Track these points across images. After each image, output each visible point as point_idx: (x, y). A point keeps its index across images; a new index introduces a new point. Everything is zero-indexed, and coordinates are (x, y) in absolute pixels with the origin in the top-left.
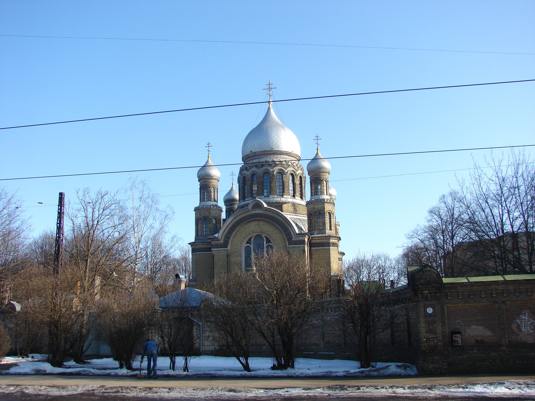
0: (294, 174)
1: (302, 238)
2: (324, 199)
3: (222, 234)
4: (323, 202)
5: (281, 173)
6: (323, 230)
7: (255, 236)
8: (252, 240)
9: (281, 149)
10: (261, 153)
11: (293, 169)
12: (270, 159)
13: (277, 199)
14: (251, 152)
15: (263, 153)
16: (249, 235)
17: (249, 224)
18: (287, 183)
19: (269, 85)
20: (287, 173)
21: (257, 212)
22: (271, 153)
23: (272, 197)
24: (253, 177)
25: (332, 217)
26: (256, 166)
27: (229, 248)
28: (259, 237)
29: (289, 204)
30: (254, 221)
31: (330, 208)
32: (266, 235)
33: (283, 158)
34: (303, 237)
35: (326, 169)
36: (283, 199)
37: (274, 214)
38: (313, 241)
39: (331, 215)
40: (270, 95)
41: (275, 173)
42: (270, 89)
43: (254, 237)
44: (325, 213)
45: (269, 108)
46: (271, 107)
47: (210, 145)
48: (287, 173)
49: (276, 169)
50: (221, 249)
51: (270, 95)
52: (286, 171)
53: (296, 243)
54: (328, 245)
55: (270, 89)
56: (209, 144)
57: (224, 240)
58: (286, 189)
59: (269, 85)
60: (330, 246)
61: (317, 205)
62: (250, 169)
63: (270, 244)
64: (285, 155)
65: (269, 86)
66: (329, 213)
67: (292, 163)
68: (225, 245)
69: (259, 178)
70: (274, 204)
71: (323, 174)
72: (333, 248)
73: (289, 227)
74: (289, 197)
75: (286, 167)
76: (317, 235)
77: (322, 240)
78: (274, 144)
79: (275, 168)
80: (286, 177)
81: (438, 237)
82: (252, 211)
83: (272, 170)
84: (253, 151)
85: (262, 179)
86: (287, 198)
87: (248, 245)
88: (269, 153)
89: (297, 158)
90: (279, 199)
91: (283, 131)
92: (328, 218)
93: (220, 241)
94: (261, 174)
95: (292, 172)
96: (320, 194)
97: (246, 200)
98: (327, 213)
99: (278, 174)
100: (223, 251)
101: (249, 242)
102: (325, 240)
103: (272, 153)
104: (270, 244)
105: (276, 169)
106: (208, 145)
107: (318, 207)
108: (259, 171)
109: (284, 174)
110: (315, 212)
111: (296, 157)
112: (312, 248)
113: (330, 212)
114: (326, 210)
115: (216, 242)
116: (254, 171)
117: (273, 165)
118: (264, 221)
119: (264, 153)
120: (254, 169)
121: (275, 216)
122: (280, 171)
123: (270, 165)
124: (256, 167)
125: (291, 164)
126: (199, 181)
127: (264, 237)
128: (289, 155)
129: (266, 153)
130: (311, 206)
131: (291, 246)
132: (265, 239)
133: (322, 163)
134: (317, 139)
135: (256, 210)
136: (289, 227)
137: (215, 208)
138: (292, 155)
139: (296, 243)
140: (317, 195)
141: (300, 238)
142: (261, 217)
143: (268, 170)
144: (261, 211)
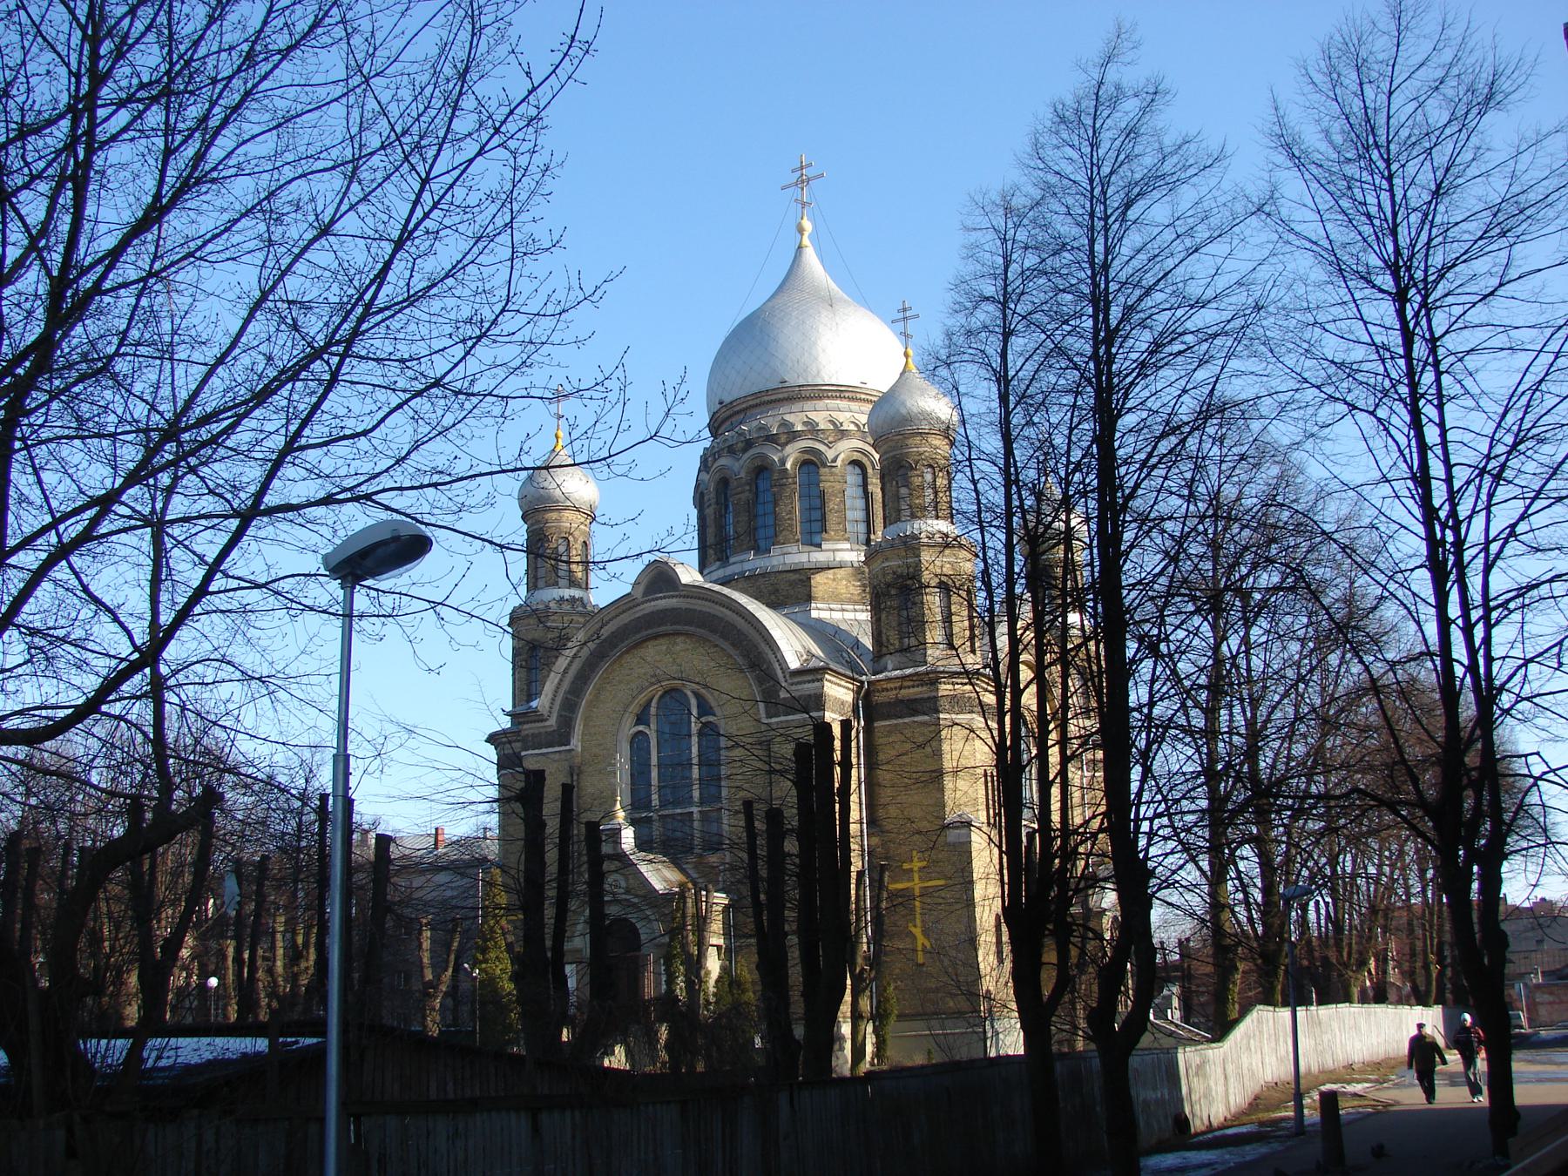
0: (865, 460)
1: (810, 685)
2: (915, 537)
3: (550, 696)
4: (911, 545)
5: (812, 463)
7: (662, 697)
8: (653, 710)
10: (751, 403)
11: (860, 444)
13: (797, 556)
14: (721, 403)
15: (754, 402)
16: (640, 693)
17: (641, 652)
19: (802, 168)
20: (834, 460)
21: (663, 604)
22: (781, 396)
23: (779, 551)
26: (731, 450)
27: (576, 743)
28: (673, 695)
29: (841, 573)
30: (656, 637)
32: (695, 687)
33: (820, 414)
34: (817, 684)
36: (819, 557)
37: (717, 607)
38: (879, 698)
40: (804, 204)
41: (788, 466)
42: (802, 182)
43: (658, 703)
45: (800, 247)
46: (806, 241)
47: (908, 314)
48: (834, 460)
49: (791, 456)
50: (550, 750)
52: (830, 454)
54: (931, 706)
55: (802, 182)
56: (904, 310)
57: (560, 716)
58: (832, 519)
59: (802, 168)
60: (938, 712)
62: (715, 460)
63: (711, 719)
64: (832, 398)
67: (857, 425)
68: (562, 735)
70: (784, 575)
73: (767, 649)
75: (831, 439)
78: (790, 364)
79: (789, 449)
80: (832, 474)
81: (1299, 633)
82: (646, 601)
84: (727, 400)
85: (747, 494)
86: (834, 551)
87: (641, 728)
88: (773, 397)
90: (803, 558)
91: (824, 313)
93: (546, 720)
94: (743, 475)
95: (856, 456)
97: (732, 560)
100: (557, 756)
101: (642, 719)
103: (786, 395)
104: (711, 719)
108: (736, 467)
109: (824, 465)
114: (926, 577)
115: (533, 725)
116: (723, 468)
117: (783, 439)
118: (687, 634)
119: (758, 401)
121: (720, 615)
122: (807, 456)
123: (771, 439)
125: (852, 427)
126: (524, 518)
127: (689, 693)
128: (850, 399)
129: (766, 398)
130: (877, 565)
131: (774, 720)
132: (693, 702)
134: (905, 318)
135: (657, 599)
136: (767, 649)
137: (566, 607)
138: (863, 396)
140: (898, 520)
141: (806, 686)
142: (674, 624)
143: (764, 457)
144: (675, 600)
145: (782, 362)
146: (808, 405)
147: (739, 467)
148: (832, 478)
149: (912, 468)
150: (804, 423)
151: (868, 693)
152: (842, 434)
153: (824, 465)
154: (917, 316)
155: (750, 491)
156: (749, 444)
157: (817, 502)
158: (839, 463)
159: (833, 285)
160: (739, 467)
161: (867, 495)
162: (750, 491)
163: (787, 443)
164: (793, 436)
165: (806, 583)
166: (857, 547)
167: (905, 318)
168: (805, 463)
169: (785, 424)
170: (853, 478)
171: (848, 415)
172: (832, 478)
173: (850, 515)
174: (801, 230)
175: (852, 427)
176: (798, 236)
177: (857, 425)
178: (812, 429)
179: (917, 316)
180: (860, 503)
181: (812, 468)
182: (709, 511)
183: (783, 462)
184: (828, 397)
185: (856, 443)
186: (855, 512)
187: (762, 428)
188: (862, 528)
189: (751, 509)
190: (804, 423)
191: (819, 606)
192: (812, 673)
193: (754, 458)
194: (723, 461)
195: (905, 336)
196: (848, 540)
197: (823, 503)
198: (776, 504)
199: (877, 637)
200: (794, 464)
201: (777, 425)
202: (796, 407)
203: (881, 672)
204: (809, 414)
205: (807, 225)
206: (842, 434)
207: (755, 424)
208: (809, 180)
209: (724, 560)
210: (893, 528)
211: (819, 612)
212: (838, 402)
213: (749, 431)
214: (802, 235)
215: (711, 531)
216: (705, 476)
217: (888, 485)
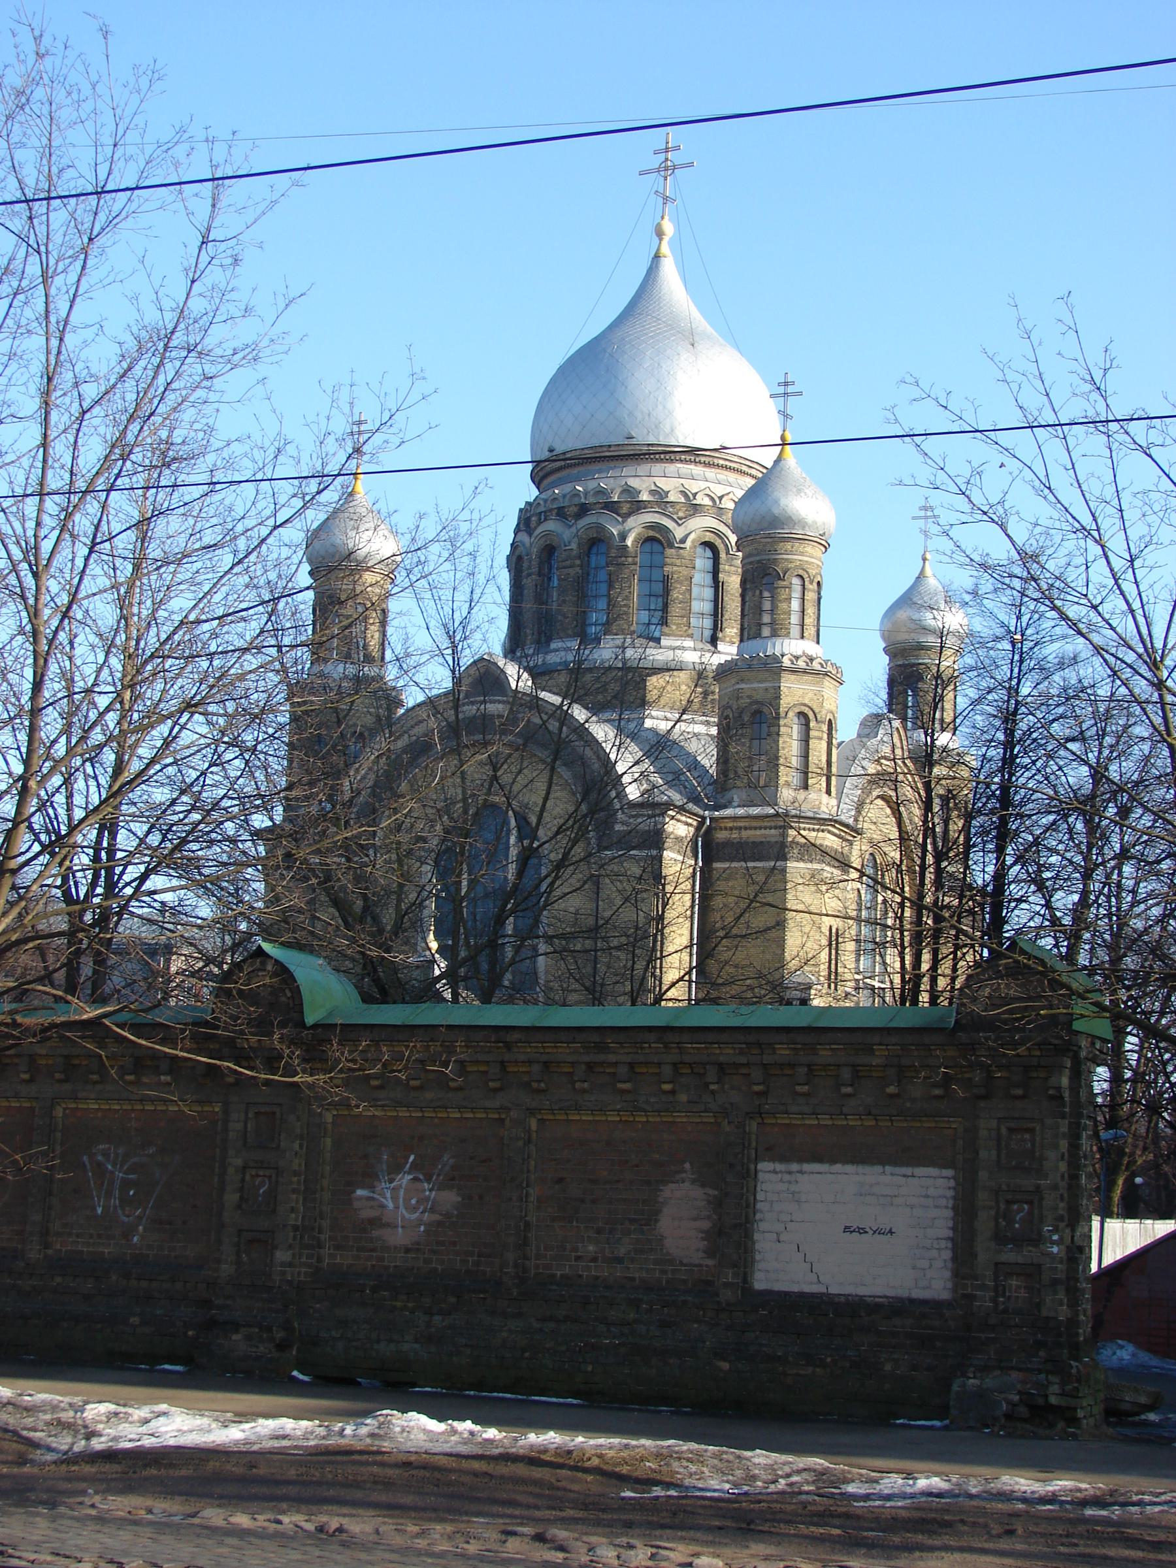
0: (718, 542)
2: (777, 659)
4: (772, 668)
6: (765, 790)
9: (667, 436)
12: (611, 482)
18: (681, 583)
19: (667, 150)
20: (683, 541)
24: (590, 549)
25: (812, 733)
26: (561, 513)
31: (810, 695)
35: (803, 524)
36: (657, 655)
38: (721, 836)
39: (812, 724)
40: (666, 199)
41: (629, 542)
42: (666, 169)
44: (778, 718)
45: (657, 256)
46: (665, 249)
47: (790, 389)
48: (683, 541)
49: (634, 529)
51: (666, 199)
52: (679, 533)
53: (626, 842)
54: (781, 851)
56: (786, 384)
58: (675, 610)
59: (667, 150)
60: (786, 859)
61: (749, 681)
62: (540, 523)
65: (662, 157)
66: (801, 714)
67: (712, 499)
69: (568, 563)
71: (788, 546)
72: (801, 865)
74: (689, 643)
75: (681, 514)
76: (741, 811)
77: (758, 832)
78: (640, 417)
79: (632, 522)
80: (680, 557)
83: (620, 527)
84: (560, 448)
85: (578, 570)
89: (754, 472)
92: (795, 735)
94: (574, 546)
95: (709, 537)
96: (766, 631)
97: (553, 646)
98: (791, 714)
99: (648, 545)
102: (767, 832)
105: (634, 529)
106: (781, 390)
107: (754, 689)
109: (671, 546)
110: (741, 712)
111: (744, 468)
112: (716, 865)
113: (806, 710)
114: (785, 702)
116: (548, 534)
117: (625, 509)
120: (551, 525)
122: (651, 533)
123: (611, 507)
124: (558, 515)
125: (707, 501)
133: (783, 502)
134: (786, 394)
138: (721, 462)
139: (626, 842)
140: (758, 635)
143: (600, 528)
145: (631, 414)
146: (657, 468)
147: (568, 534)
148: (678, 562)
149: (780, 579)
150: (652, 492)
151: (710, 828)
152: (695, 509)
153: (671, 546)
154: (800, 394)
155: (581, 566)
156: (583, 510)
157: (658, 588)
158: (688, 544)
159: (696, 314)
160: (568, 534)
161: (717, 585)
162: (581, 566)
163: (629, 515)
164: (638, 506)
165: (641, 685)
166: (700, 645)
167: (786, 394)
168: (650, 540)
169: (628, 490)
170: (703, 562)
171: (703, 485)
172: (678, 562)
173: (697, 606)
174: (660, 234)
175: (707, 501)
176: (656, 240)
177: (712, 499)
178: (660, 499)
179: (800, 394)
180: (709, 593)
181: (657, 547)
182: (529, 582)
183: (623, 537)
184: (681, 461)
185: (711, 522)
186: (702, 604)
187: (601, 492)
188: (708, 623)
189: (581, 589)
190: (652, 492)
191: (654, 713)
192: (653, 808)
193: (589, 528)
194: (551, 525)
195: (785, 415)
196: (691, 636)
197: (666, 592)
198: (611, 586)
199: (723, 759)
200: (635, 541)
201: (618, 490)
202: (643, 469)
203: (725, 807)
204: (657, 480)
205: (668, 227)
206: (695, 509)
207: (592, 485)
208: (674, 168)
209: (543, 640)
210: (753, 646)
211: (657, 721)
212: (692, 466)
213: (586, 493)
214: (661, 240)
215: (528, 605)
216: (524, 537)
217: (750, 594)
